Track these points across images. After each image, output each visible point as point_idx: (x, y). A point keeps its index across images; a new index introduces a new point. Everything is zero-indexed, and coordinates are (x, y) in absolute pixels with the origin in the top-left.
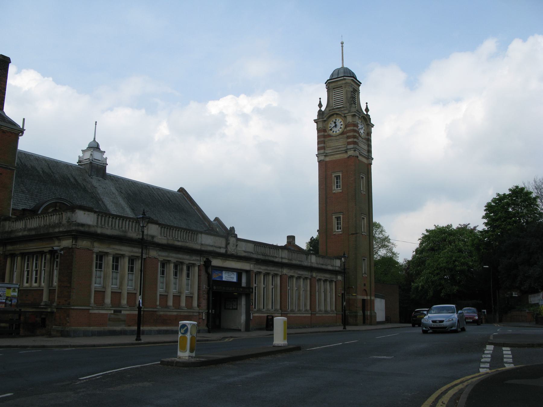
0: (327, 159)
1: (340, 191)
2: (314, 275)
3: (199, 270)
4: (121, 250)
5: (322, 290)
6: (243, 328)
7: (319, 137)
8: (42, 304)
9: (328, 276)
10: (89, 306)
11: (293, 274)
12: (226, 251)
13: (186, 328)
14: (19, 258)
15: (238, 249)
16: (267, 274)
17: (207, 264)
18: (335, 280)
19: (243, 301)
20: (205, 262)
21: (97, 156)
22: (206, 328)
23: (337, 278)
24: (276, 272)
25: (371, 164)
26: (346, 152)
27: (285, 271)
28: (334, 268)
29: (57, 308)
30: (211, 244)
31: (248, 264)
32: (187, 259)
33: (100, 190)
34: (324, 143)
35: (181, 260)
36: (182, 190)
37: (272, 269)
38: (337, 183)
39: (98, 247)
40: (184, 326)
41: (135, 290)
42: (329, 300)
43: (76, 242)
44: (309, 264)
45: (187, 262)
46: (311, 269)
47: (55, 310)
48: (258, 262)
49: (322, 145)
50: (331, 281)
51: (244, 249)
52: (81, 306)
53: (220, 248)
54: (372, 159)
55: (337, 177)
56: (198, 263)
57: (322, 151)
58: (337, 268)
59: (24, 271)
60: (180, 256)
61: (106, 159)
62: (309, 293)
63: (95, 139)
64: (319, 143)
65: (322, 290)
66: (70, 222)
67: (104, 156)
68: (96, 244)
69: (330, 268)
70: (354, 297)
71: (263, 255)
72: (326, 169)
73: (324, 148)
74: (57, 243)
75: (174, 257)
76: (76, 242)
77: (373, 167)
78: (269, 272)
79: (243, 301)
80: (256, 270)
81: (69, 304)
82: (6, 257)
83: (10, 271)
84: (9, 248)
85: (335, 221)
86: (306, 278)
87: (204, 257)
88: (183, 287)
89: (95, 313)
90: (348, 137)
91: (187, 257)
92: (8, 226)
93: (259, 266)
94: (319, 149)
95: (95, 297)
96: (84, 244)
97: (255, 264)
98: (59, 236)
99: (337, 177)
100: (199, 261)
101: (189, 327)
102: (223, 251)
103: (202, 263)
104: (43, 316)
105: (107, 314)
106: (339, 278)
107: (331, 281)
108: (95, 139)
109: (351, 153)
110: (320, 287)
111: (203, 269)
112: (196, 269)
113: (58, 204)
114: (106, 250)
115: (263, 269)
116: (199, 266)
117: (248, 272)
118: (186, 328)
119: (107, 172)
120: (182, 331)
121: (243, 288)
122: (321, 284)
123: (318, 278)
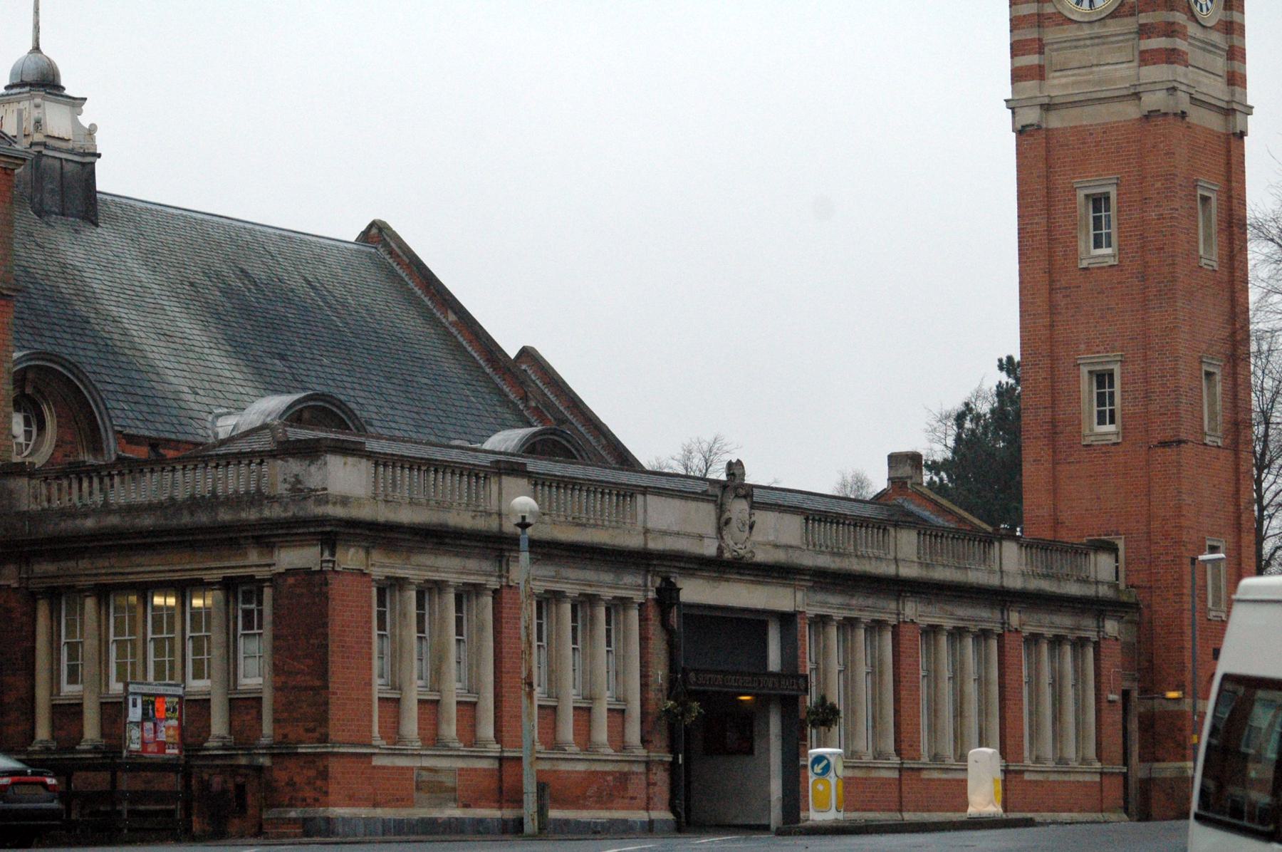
0: (1055, 121)
1: (1112, 262)
2: (1014, 618)
3: (643, 619)
4: (437, 570)
5: (1046, 678)
6: (775, 817)
7: (1015, 23)
8: (84, 746)
9: (1062, 622)
10: (371, 746)
11: (935, 621)
12: (720, 549)
13: (825, 762)
14: (90, 603)
15: (757, 536)
16: (848, 624)
17: (667, 595)
18: (1093, 635)
19: (775, 725)
20: (658, 591)
21: (57, 121)
22: (669, 816)
23: (1100, 628)
24: (877, 616)
25: (1242, 134)
26: (1137, 96)
27: (912, 609)
28: (1089, 591)
29: (273, 756)
30: (675, 529)
31: (789, 591)
32: (607, 584)
33: (97, 281)
34: (1041, 52)
35: (590, 591)
36: (378, 234)
37: (865, 607)
38: (1097, 224)
39: (383, 565)
40: (819, 759)
41: (394, 688)
42: (1069, 718)
43: (333, 554)
44: (994, 581)
45: (607, 594)
46: (1001, 598)
47: (265, 761)
48: (825, 580)
49: (1032, 60)
50: (1079, 644)
51: (771, 538)
52: (353, 745)
53: (701, 537)
54: (1249, 110)
55: (1099, 202)
56: (638, 597)
57: (1030, 86)
58: (1104, 591)
59: (107, 642)
60: (590, 575)
61: (91, 131)
62: (995, 689)
63: (37, 48)
64: (1017, 49)
65: (1046, 678)
66: (299, 491)
67: (85, 120)
68: (376, 556)
69: (1073, 589)
70: (1172, 707)
71: (833, 554)
72: (1046, 160)
73: (1039, 73)
74: (254, 557)
75: (574, 580)
76: (333, 554)
77: (1251, 145)
78: (854, 614)
79: (775, 725)
80: (812, 611)
81: (324, 739)
82: (32, 597)
83: (51, 642)
84: (45, 568)
85: (1087, 389)
86: (984, 635)
87: (656, 574)
88: (605, 678)
89: (384, 768)
90: (1144, 31)
91: (608, 577)
92: (27, 496)
93: (820, 597)
94: (1018, 75)
95: (380, 717)
96: (350, 558)
97: (809, 588)
98: (269, 535)
99: (1099, 202)
100: (636, 587)
101: (832, 760)
102: (710, 549)
103: (652, 595)
104: (239, 780)
105: (411, 769)
106: (1111, 627)
107: (1079, 644)
108: (37, 48)
109: (1154, 100)
110: (1038, 663)
111: (653, 614)
112: (634, 615)
113: (30, 376)
114: (400, 573)
115: (834, 605)
116: (641, 605)
117: (787, 620)
118: (825, 762)
119: (101, 185)
120: (818, 769)
121: (773, 674)
122: (1038, 654)
123: (1027, 630)
